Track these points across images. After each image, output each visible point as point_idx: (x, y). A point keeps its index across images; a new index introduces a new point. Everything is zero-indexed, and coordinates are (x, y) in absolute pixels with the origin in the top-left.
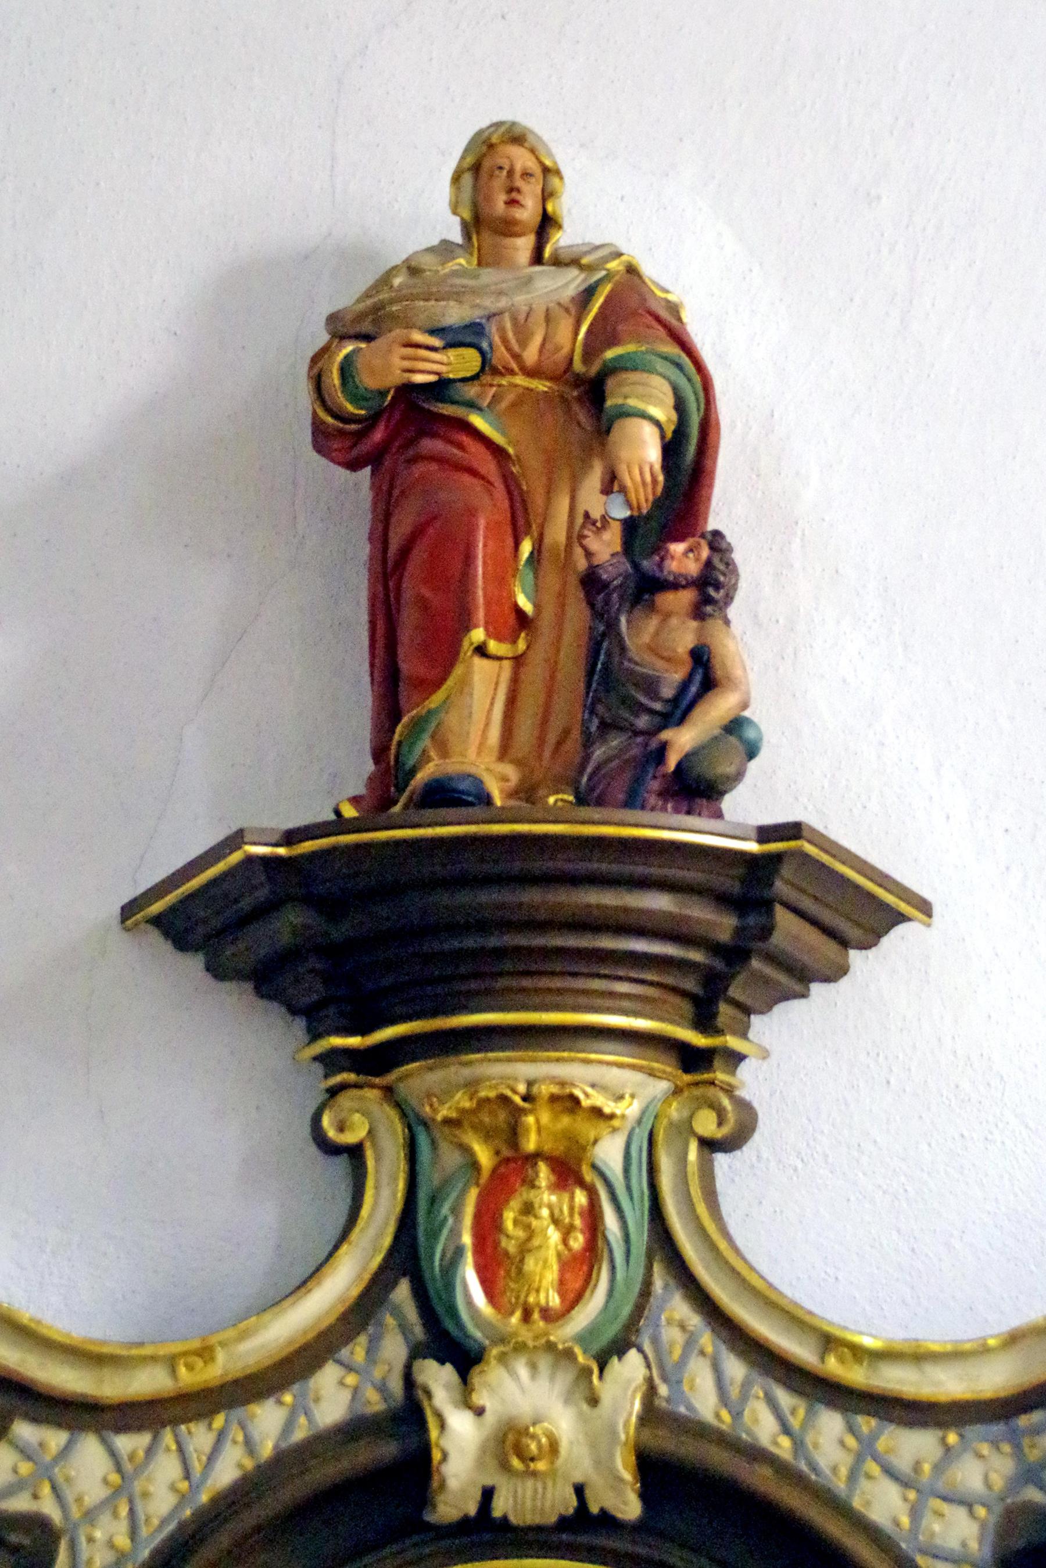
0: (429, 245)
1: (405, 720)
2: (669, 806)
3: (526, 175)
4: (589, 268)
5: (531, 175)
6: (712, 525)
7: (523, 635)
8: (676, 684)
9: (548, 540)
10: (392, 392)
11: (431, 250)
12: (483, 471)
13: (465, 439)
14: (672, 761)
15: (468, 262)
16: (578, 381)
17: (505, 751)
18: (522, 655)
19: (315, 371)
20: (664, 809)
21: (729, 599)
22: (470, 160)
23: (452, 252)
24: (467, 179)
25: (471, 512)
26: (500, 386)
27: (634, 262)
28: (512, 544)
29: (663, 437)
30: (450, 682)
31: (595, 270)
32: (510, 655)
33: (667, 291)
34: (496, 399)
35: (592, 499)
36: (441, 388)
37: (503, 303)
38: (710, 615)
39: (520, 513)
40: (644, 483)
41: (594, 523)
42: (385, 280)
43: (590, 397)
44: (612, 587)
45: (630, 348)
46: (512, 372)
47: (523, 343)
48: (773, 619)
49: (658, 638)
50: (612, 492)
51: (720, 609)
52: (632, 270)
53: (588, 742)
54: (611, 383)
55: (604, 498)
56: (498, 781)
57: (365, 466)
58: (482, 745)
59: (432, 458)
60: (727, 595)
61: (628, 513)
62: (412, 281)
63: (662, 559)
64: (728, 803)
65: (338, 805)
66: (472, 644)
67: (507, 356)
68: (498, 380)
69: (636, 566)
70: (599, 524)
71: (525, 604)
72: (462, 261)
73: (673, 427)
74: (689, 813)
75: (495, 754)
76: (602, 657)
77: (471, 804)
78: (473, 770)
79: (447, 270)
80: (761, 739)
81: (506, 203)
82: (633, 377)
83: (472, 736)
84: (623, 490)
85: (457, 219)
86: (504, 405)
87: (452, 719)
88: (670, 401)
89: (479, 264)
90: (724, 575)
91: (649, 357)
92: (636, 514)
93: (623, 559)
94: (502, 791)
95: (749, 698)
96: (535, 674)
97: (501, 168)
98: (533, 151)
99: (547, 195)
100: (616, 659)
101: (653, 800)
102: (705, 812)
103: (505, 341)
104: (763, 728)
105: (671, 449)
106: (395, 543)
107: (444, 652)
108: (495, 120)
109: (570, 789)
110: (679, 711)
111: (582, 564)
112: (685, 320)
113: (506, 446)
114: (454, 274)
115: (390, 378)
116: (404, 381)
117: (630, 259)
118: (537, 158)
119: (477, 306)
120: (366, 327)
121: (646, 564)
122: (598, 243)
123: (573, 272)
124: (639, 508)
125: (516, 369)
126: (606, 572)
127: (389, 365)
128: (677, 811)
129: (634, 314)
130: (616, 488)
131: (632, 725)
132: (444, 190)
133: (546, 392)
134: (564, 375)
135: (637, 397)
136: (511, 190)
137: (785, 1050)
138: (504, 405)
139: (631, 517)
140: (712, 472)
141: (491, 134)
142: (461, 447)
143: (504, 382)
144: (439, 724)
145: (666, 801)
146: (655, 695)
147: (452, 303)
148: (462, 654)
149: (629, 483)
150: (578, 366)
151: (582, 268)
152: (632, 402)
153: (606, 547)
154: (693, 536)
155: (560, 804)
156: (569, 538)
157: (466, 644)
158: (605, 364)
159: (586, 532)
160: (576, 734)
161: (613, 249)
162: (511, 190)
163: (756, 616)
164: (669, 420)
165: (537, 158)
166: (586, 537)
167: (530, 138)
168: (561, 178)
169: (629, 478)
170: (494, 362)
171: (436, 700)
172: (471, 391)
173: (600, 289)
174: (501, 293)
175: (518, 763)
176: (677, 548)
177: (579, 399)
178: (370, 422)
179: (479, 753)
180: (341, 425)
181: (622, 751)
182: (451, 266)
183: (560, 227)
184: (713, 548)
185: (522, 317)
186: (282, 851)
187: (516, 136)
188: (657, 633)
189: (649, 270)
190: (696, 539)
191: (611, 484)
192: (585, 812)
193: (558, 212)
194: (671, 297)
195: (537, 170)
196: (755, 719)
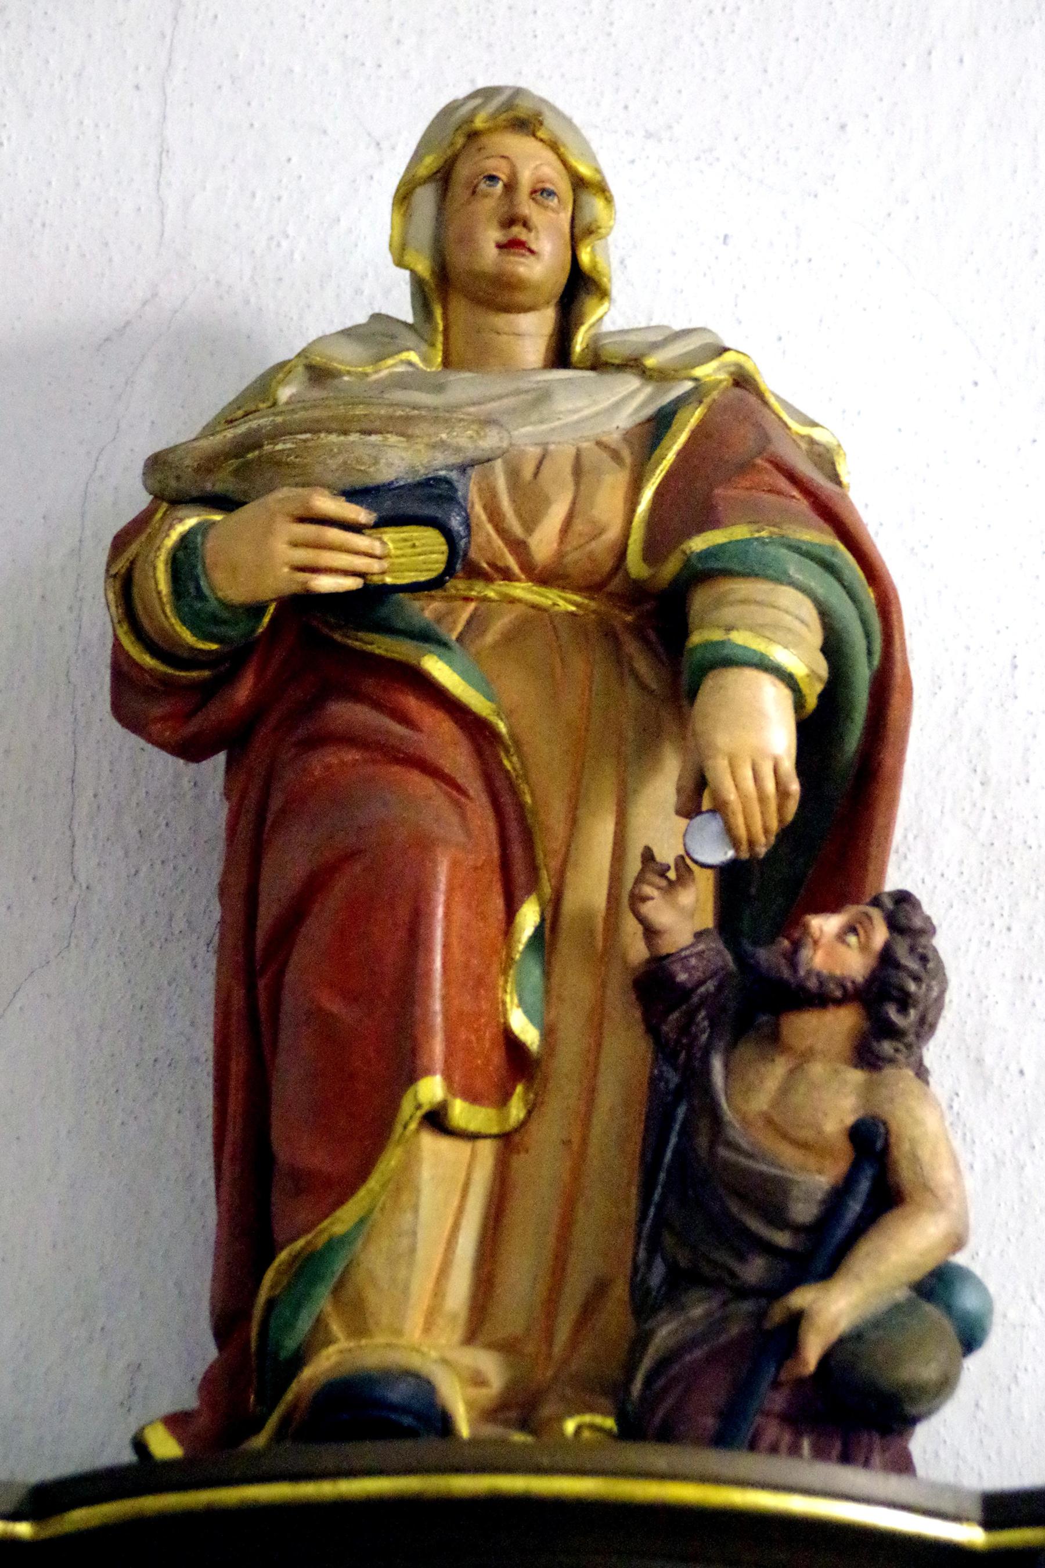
0: (349, 324)
1: (283, 1256)
2: (806, 1444)
3: (541, 192)
4: (660, 377)
5: (551, 193)
6: (893, 881)
7: (519, 1089)
8: (820, 1196)
9: (571, 904)
10: (272, 609)
11: (348, 333)
12: (447, 766)
13: (412, 703)
14: (813, 1350)
15: (425, 359)
16: (636, 594)
17: (475, 1332)
18: (516, 1130)
19: (121, 565)
20: (794, 1450)
21: (926, 1026)
22: (430, 163)
23: (393, 337)
24: (426, 198)
25: (424, 845)
26: (485, 599)
27: (749, 366)
28: (501, 916)
29: (799, 704)
30: (373, 1183)
31: (674, 378)
32: (495, 1130)
33: (814, 424)
34: (476, 625)
35: (659, 825)
36: (370, 603)
37: (491, 440)
38: (891, 1061)
39: (517, 850)
40: (762, 799)
41: (663, 872)
42: (263, 389)
43: (654, 631)
44: (695, 999)
45: (740, 532)
46: (507, 575)
47: (530, 523)
48: (1014, 1068)
49: (792, 1103)
50: (698, 812)
51: (909, 1046)
52: (743, 380)
53: (645, 1306)
54: (700, 599)
55: (682, 823)
56: (464, 1384)
57: (215, 752)
58: (432, 1314)
59: (350, 739)
60: (922, 1020)
61: (731, 854)
62: (316, 393)
63: (797, 946)
64: (924, 1441)
65: (142, 1429)
66: (419, 1107)
67: (498, 542)
68: (479, 589)
69: (741, 958)
70: (672, 875)
71: (526, 1031)
72: (413, 356)
73: (819, 688)
74: (846, 1458)
75: (458, 1333)
76: (673, 1140)
77: (410, 1433)
78: (415, 1362)
79: (384, 373)
80: (989, 1311)
81: (500, 246)
82: (743, 588)
83: (415, 1287)
84: (720, 808)
85: (407, 273)
86: (490, 637)
87: (374, 1260)
88: (815, 637)
89: (446, 363)
90: (917, 979)
91: (772, 550)
92: (745, 855)
93: (717, 944)
94: (470, 1405)
95: (966, 1227)
96: (543, 1167)
97: (492, 178)
98: (554, 146)
99: (579, 233)
100: (702, 1141)
101: (772, 1430)
102: (877, 1459)
103: (495, 515)
104: (992, 1288)
105: (816, 729)
106: (267, 915)
107: (364, 1125)
108: (481, 84)
109: (604, 1402)
110: (826, 1248)
111: (637, 951)
112: (844, 479)
113: (494, 719)
114: (400, 382)
115: (270, 581)
116: (295, 588)
117: (741, 359)
118: (565, 163)
119: (442, 445)
120: (221, 483)
121: (765, 956)
122: (677, 327)
123: (631, 382)
124: (751, 843)
125: (516, 568)
126: (687, 969)
127: (289, 550)
128: (820, 1453)
129: (746, 467)
130: (706, 804)
131: (733, 1275)
132: (375, 221)
133: (572, 614)
134: (607, 582)
135: (751, 629)
136: (510, 221)
138: (490, 637)
139: (734, 863)
140: (895, 779)
141: (475, 111)
142: (404, 718)
143: (492, 594)
144: (351, 1262)
145: (798, 1434)
146: (777, 1217)
147: (393, 439)
148: (398, 1129)
149: (732, 796)
150: (635, 565)
151: (645, 374)
152: (739, 638)
153: (685, 917)
154: (857, 901)
155: (586, 1434)
156: (613, 898)
157: (407, 1107)
158: (688, 562)
159: (647, 890)
160: (620, 1290)
161: (707, 339)
162: (510, 221)
163: (979, 1061)
164: (813, 674)
165: (565, 163)
166: (645, 899)
167: (549, 120)
168: (609, 200)
169: (734, 784)
170: (473, 554)
171: (343, 1219)
172: (427, 610)
173: (680, 416)
174: (488, 422)
175: (507, 1348)
176: (826, 925)
177: (638, 631)
178: (227, 666)
179: (427, 1329)
180: (170, 671)
181: (716, 1324)
182: (393, 366)
183: (603, 294)
184: (895, 926)
185: (528, 472)
186: (23, 1529)
187: (523, 118)
188: (785, 1090)
189: (772, 380)
190: (862, 908)
191: (697, 796)
192: (634, 1454)
193: (602, 265)
194: (816, 434)
195: (564, 186)
196: (977, 1269)
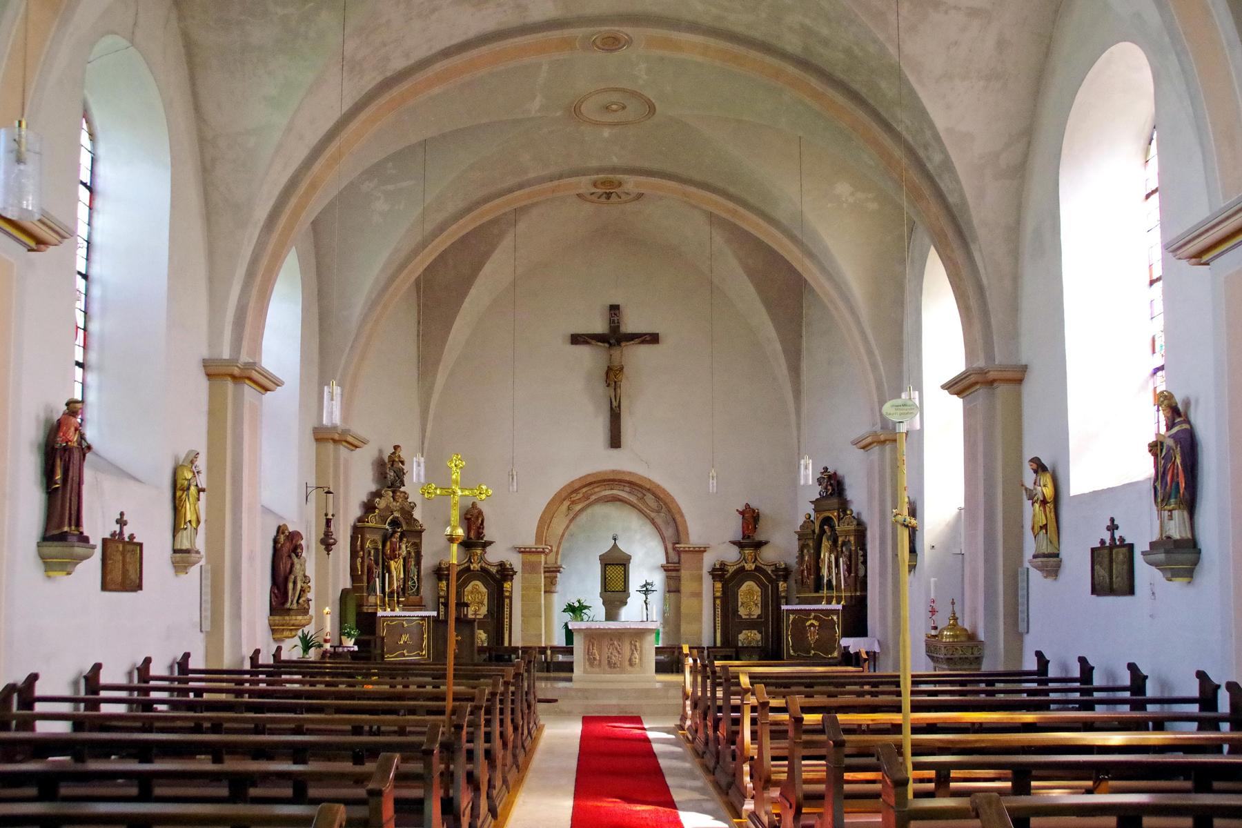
43: (477, 518)
137: (488, 549)
